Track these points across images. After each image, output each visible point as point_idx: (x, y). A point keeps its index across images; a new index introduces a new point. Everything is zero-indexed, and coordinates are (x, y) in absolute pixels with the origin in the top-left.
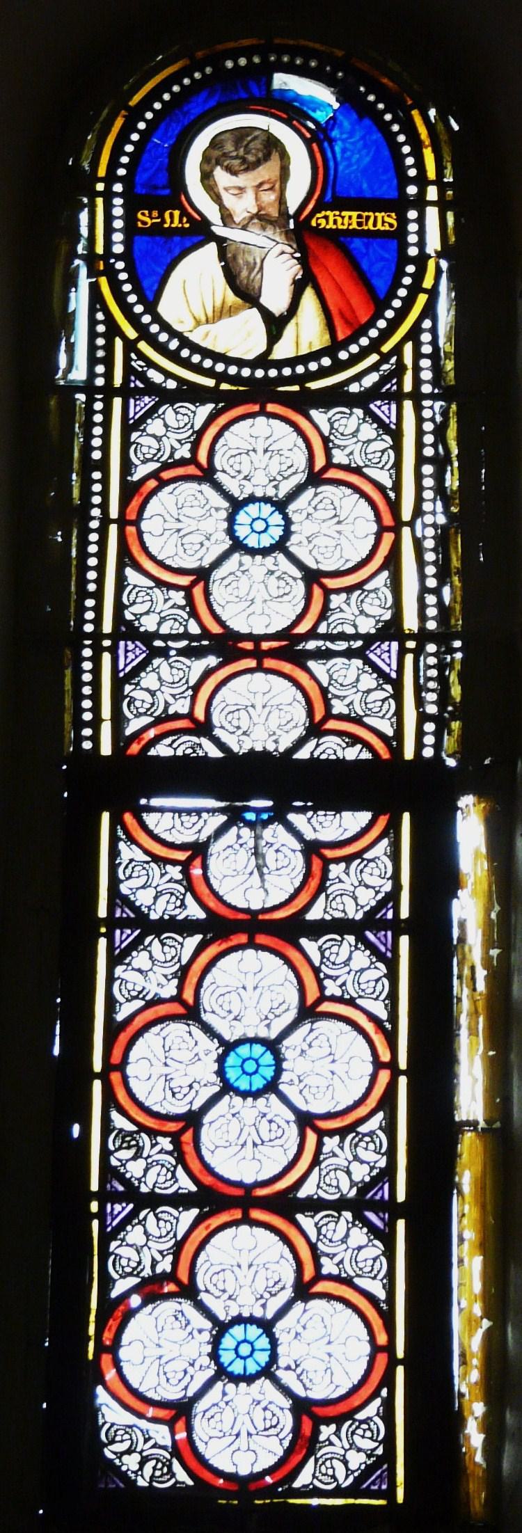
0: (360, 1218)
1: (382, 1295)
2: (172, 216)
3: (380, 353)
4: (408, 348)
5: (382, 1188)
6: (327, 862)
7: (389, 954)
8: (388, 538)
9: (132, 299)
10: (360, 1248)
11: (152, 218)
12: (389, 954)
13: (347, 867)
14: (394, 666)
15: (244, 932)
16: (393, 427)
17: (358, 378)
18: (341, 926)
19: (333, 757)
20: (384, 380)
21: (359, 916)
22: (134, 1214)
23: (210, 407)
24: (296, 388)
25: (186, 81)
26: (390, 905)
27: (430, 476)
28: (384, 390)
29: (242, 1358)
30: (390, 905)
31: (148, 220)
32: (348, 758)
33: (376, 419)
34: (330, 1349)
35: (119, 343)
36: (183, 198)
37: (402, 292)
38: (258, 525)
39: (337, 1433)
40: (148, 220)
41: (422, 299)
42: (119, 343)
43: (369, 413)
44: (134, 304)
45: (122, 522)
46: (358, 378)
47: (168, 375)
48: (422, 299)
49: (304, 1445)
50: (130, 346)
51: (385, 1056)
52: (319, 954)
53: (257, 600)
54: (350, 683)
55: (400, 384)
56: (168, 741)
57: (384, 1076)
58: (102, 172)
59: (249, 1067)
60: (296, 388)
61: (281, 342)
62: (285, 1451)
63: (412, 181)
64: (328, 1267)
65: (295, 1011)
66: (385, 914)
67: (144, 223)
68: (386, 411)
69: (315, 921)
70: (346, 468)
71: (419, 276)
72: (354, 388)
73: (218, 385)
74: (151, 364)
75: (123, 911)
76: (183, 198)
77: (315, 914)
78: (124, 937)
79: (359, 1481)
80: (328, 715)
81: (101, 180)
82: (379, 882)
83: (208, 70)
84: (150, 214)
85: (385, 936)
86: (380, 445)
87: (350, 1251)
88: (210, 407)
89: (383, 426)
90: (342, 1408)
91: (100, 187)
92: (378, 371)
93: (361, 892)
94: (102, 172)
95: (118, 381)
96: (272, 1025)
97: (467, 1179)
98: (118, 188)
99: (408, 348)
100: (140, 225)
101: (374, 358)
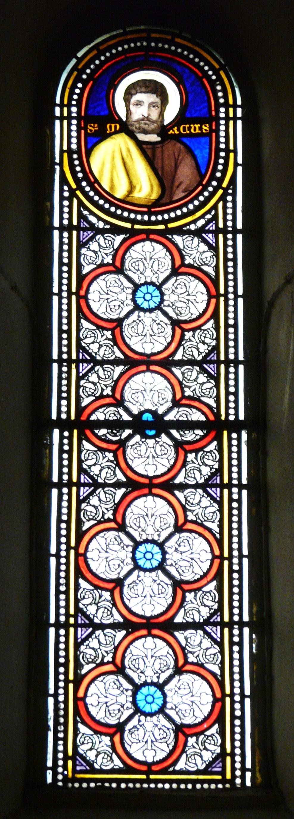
0: (204, 371)
1: (214, 405)
4: (220, 205)
5: (216, 479)
6: (183, 397)
7: (82, 221)
8: (213, 301)
10: (207, 649)
12: (82, 221)
13: (194, 334)
14: (218, 495)
15: (143, 234)
16: (218, 499)
17: (194, 222)
18: (192, 362)
19: (185, 419)
21: (200, 358)
22: (92, 368)
23: (122, 237)
26: (218, 474)
29: (147, 301)
30: (218, 474)
31: (92, 129)
32: (193, 419)
33: (209, 495)
34: (192, 699)
35: (75, 201)
38: (149, 699)
39: (193, 336)
40: (92, 129)
42: (75, 201)
43: (206, 633)
45: (77, 294)
46: (194, 222)
49: (178, 749)
50: (81, 204)
51: (213, 291)
52: (181, 376)
53: (147, 336)
54: (197, 382)
55: (217, 224)
56: (101, 410)
57: (217, 562)
59: (148, 297)
62: (168, 606)
63: (222, 150)
64: (188, 335)
65: (170, 270)
66: (217, 619)
67: (91, 130)
68: (211, 368)
69: (179, 360)
70: (195, 522)
72: (192, 227)
74: (92, 213)
75: (84, 224)
77: (178, 356)
78: (84, 368)
79: (208, 766)
80: (186, 662)
82: (210, 341)
85: (214, 367)
86: (209, 385)
87: (196, 344)
88: (122, 237)
89: (210, 376)
90: (197, 446)
93: (203, 504)
95: (75, 222)
96: (161, 534)
99: (220, 205)
100: (89, 131)
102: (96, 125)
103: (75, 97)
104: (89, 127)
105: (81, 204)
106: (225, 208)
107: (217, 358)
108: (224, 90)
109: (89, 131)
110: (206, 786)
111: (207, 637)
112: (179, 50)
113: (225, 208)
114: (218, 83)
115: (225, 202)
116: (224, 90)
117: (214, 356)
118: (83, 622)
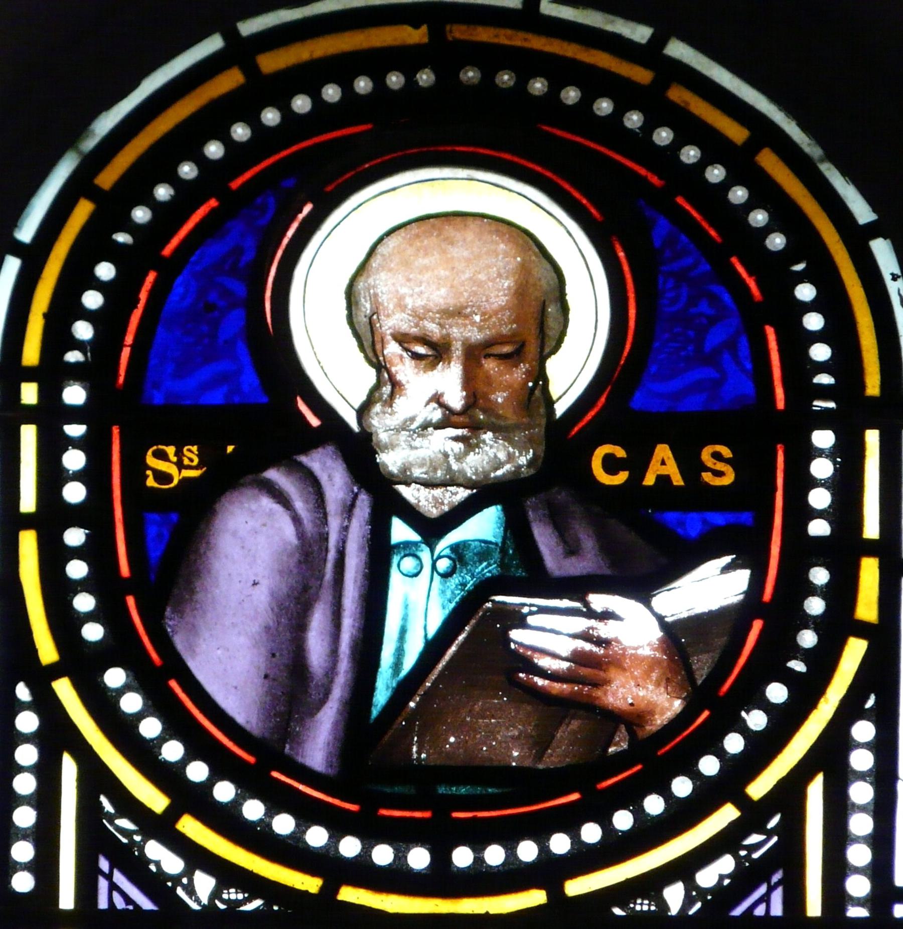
3: (743, 802)
4: (815, 790)
7: (104, 864)
9: (150, 728)
11: (180, 466)
12: (104, 864)
20: (746, 878)
25: (363, 85)
28: (738, 912)
31: (172, 470)
35: (69, 768)
40: (172, 470)
41: (855, 651)
42: (69, 768)
44: (121, 692)
48: (855, 651)
58: (31, 354)
71: (843, 592)
81: (30, 374)
83: (425, 78)
84: (179, 453)
91: (29, 393)
94: (31, 354)
98: (75, 395)
99: (815, 790)
101: (728, 814)
102: (192, 453)
103: (83, 330)
104: (151, 461)
105: (96, 777)
106: (838, 809)
107: (787, 902)
108: (833, 301)
109: (151, 482)
110: (25, 817)
111: (559, 766)
112: (604, 106)
113: (838, 809)
114: (799, 267)
115: (839, 781)
116: (833, 301)
117: (766, 899)
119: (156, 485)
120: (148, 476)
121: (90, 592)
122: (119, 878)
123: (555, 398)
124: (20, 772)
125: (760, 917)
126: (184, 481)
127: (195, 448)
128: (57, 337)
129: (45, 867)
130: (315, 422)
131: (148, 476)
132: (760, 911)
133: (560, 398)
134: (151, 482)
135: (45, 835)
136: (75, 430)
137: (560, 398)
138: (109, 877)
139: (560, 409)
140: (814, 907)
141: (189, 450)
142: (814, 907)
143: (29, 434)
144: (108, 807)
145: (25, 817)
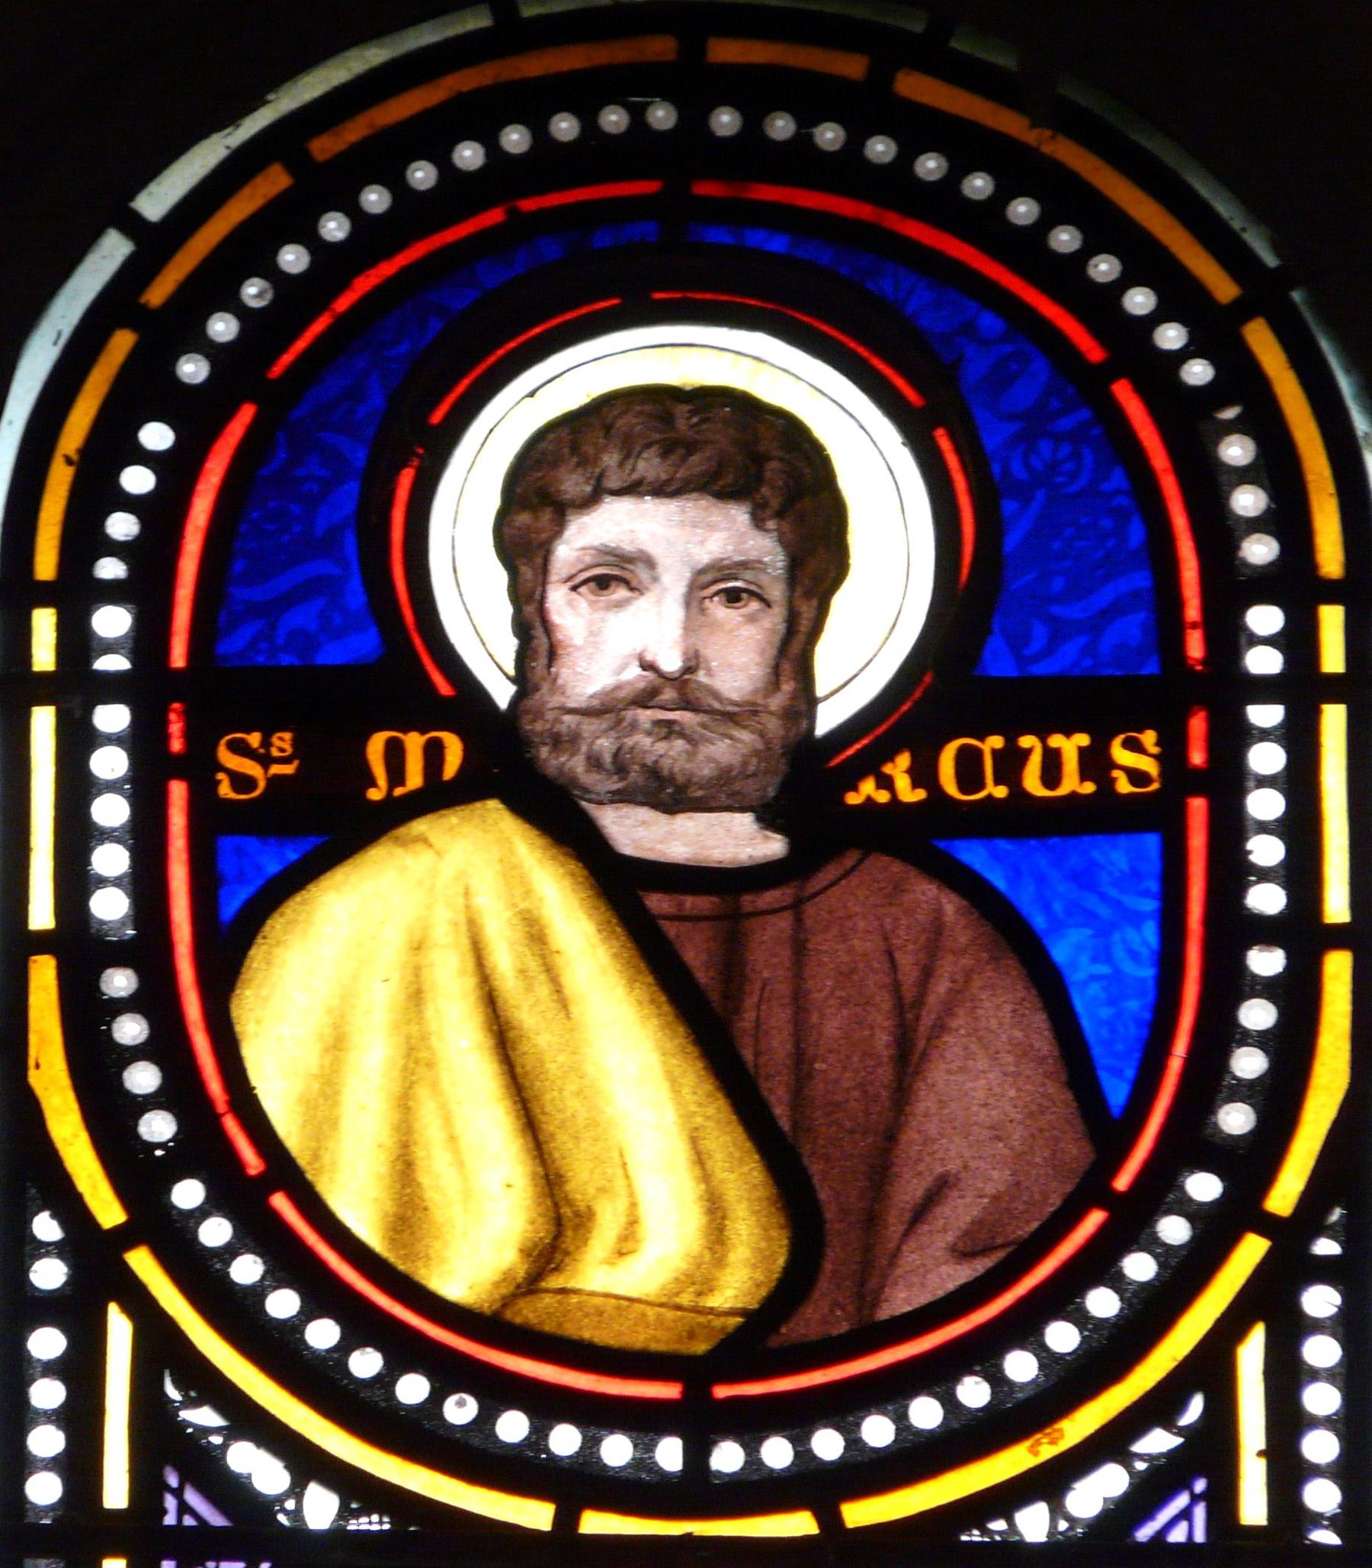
2: (395, 754)
4: (1251, 1355)
17: (1049, 1482)
20: (1153, 1488)
24: (800, 1524)
27: (102, 882)
35: (119, 1329)
36: (406, 479)
37: (777, 1453)
42: (119, 1329)
46: (1049, 1482)
47: (307, 1463)
50: (160, 1346)
60: (800, 1524)
61: (493, 550)
67: (242, 782)
73: (566, 1519)
74: (250, 1421)
75: (184, 1508)
76: (406, 479)
92: (1125, 1458)
97: (852, 345)
99: (1251, 1355)
102: (283, 742)
105: (160, 1346)
106: (1286, 1376)
109: (225, 790)
113: (1286, 1376)
114: (1230, 413)
118: (188, 1521)
119: (233, 796)
120: (219, 782)
121: (107, 537)
122: (192, 1497)
123: (820, 691)
124: (54, 1459)
125: (1178, 1545)
126: (274, 781)
127: (287, 736)
128: (83, 539)
129: (81, 1465)
130: (437, 417)
131: (219, 782)
132: (1178, 1535)
133: (827, 697)
134: (225, 790)
135: (82, 1419)
136: (114, 663)
137: (827, 697)
138: (178, 1493)
139: (828, 719)
140: (1253, 1507)
141: (281, 739)
142: (1253, 1507)
143: (43, 721)
144: (172, 1392)
145: (48, 1394)
